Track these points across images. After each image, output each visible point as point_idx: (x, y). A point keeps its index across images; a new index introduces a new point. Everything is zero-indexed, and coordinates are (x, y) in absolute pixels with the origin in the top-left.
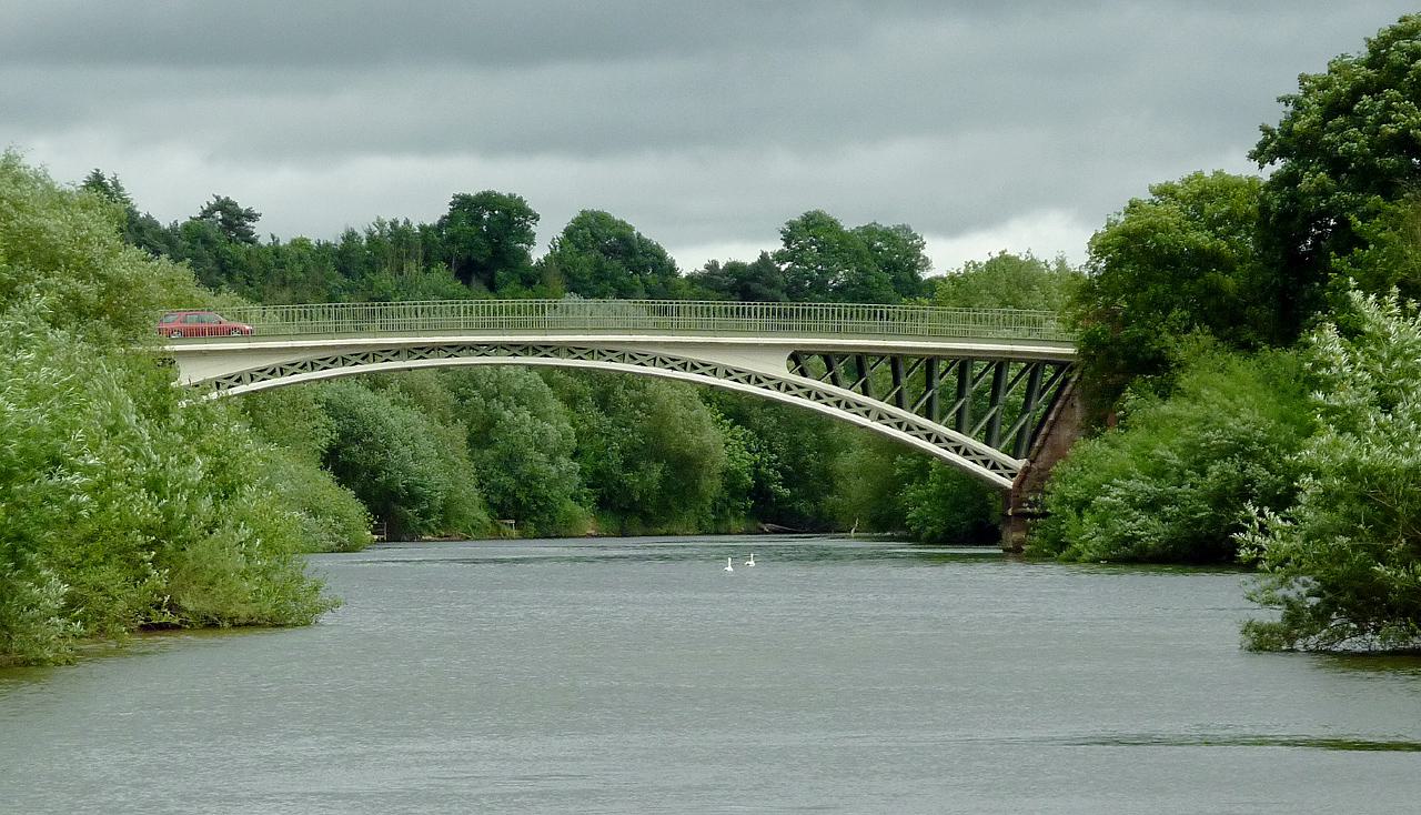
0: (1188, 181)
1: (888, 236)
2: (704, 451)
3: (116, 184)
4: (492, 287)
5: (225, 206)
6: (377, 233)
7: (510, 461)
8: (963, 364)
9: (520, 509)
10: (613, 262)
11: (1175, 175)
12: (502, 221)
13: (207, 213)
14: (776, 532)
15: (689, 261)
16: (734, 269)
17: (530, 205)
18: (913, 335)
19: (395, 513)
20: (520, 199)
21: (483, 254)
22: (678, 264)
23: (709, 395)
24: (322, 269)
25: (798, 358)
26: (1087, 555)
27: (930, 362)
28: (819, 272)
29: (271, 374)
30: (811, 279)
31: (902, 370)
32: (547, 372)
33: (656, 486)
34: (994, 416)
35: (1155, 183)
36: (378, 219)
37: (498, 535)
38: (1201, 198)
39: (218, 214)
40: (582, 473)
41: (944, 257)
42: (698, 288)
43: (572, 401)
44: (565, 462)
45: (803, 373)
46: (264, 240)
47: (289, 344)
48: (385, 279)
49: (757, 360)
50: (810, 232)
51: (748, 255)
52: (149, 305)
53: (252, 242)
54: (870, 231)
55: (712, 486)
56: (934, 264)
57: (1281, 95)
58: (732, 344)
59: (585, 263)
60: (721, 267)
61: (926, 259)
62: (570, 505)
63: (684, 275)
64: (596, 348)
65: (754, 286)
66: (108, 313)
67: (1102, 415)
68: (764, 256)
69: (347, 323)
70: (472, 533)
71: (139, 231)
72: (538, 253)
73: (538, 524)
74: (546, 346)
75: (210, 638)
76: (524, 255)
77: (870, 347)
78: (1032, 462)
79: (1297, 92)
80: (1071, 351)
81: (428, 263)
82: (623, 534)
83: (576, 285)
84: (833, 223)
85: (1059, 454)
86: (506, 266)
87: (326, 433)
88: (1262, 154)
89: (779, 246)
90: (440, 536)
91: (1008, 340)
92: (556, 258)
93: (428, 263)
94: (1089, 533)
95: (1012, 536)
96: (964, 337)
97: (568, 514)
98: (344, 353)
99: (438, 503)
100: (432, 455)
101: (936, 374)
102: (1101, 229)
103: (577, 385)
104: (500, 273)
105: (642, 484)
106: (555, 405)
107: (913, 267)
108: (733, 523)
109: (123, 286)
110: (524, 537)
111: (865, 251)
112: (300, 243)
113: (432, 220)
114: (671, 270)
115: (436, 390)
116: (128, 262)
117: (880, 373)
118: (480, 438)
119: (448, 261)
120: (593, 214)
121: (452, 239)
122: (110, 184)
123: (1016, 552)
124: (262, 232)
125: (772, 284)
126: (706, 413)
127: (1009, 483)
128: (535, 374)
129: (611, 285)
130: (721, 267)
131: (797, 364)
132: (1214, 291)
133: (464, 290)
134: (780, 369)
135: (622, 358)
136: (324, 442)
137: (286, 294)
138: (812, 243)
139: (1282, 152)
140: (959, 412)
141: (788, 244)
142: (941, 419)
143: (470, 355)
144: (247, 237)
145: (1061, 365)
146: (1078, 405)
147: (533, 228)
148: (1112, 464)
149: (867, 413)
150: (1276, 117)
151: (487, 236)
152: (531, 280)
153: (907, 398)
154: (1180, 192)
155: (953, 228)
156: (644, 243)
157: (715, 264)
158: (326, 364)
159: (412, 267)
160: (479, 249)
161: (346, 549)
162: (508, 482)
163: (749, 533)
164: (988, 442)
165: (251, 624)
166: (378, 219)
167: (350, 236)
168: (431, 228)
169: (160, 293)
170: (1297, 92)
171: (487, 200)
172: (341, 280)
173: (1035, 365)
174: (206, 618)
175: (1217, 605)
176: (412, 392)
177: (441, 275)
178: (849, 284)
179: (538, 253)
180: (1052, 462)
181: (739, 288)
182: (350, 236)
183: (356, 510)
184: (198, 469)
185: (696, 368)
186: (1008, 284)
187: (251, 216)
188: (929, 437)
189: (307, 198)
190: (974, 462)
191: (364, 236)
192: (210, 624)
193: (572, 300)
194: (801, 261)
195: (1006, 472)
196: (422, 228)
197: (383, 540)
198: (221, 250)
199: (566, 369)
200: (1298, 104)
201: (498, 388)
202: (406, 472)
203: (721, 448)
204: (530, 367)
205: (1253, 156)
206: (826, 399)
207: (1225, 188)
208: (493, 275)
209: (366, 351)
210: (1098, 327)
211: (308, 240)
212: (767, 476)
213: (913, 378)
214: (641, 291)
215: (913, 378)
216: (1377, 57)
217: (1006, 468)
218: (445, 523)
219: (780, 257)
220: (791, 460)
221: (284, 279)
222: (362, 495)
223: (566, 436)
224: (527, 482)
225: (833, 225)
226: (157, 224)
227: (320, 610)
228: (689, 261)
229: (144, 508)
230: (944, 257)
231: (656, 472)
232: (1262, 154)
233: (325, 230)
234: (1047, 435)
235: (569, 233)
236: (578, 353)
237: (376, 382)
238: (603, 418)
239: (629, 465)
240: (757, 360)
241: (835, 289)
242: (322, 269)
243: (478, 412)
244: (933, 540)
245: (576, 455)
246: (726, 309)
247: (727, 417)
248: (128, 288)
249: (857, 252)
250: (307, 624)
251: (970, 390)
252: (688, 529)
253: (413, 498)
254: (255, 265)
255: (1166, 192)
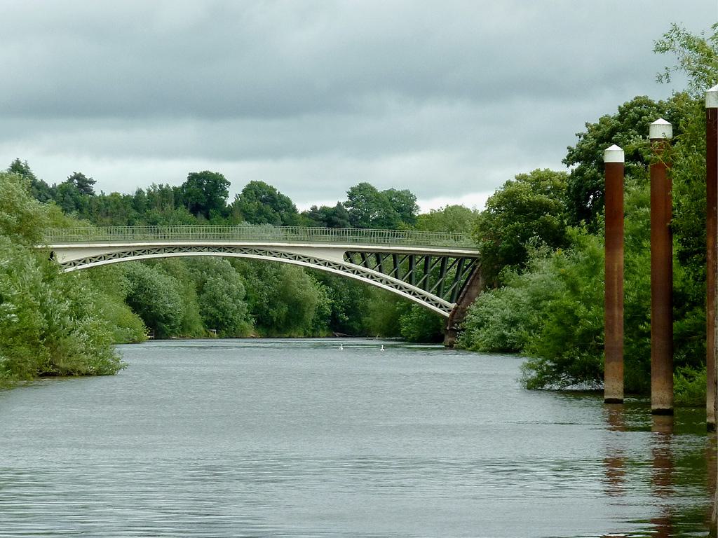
0: (533, 174)
1: (399, 195)
2: (307, 299)
3: (27, 167)
4: (208, 217)
5: (79, 177)
6: (152, 191)
7: (213, 300)
8: (427, 257)
9: (219, 325)
10: (266, 205)
11: (527, 171)
12: (213, 185)
13: (71, 180)
14: (340, 336)
15: (303, 207)
16: (324, 210)
17: (226, 177)
18: (407, 245)
19: (158, 325)
20: (221, 175)
21: (203, 201)
22: (297, 207)
23: (309, 271)
24: (125, 207)
25: (349, 255)
26: (482, 348)
27: (411, 257)
28: (366, 212)
29: (99, 259)
30: (361, 215)
31: (398, 261)
32: (232, 260)
33: (283, 317)
34: (441, 282)
35: (517, 174)
36: (153, 184)
37: (208, 337)
38: (538, 181)
39: (76, 181)
40: (248, 308)
41: (424, 207)
42: (307, 219)
43: (244, 273)
44: (241, 303)
45: (351, 262)
46: (98, 194)
47: (88, 246)
48: (156, 213)
49: (329, 255)
50: (362, 193)
51: (332, 204)
52: (41, 225)
53: (93, 194)
54: (391, 192)
55: (311, 316)
56: (421, 209)
57: (577, 133)
58: (334, 248)
59: (253, 206)
60: (318, 209)
61: (417, 206)
62: (243, 323)
63: (300, 213)
64: (254, 248)
65: (334, 218)
66: (25, 230)
67: (494, 283)
68: (339, 204)
69: (138, 235)
70: (196, 336)
71: (39, 190)
72: (230, 201)
73: (227, 332)
74: (230, 247)
75: (71, 379)
76: (223, 202)
77: (399, 250)
78: (458, 305)
79: (585, 131)
80: (478, 252)
81: (177, 204)
82: (268, 337)
83: (248, 217)
84: (372, 188)
85: (472, 300)
86: (214, 207)
87: (128, 286)
88: (569, 161)
89: (347, 199)
90: (180, 337)
91: (446, 247)
92: (238, 204)
93: (177, 204)
94: (480, 336)
95: (448, 339)
96: (428, 245)
97: (242, 327)
98: (133, 249)
99: (179, 322)
100: (174, 296)
101: (414, 262)
102: (492, 194)
103: (247, 265)
104: (211, 211)
105: (277, 314)
106: (236, 275)
107: (411, 210)
108: (321, 332)
109: (30, 217)
110: (221, 337)
111: (387, 200)
112: (115, 195)
113: (179, 185)
114: (294, 210)
115: (181, 266)
116: (32, 205)
117: (372, 260)
118: (200, 290)
119: (186, 204)
120: (257, 183)
121: (189, 194)
122: (24, 166)
123: (451, 346)
124: (97, 190)
125: (342, 217)
126: (308, 278)
127: (448, 315)
128: (226, 261)
129: (265, 217)
130: (318, 209)
131: (348, 257)
132: (546, 225)
133: (194, 219)
134: (339, 259)
135: (266, 253)
136: (125, 293)
137: (108, 220)
138: (362, 198)
139: (578, 159)
140: (425, 281)
141: (351, 198)
142: (416, 284)
143: (194, 251)
144: (89, 192)
145: (473, 258)
146: (481, 278)
147: (228, 189)
148: (493, 305)
149: (381, 281)
150: (574, 143)
151: (205, 193)
152: (227, 214)
153: (401, 273)
154: (529, 179)
155: (431, 194)
156: (281, 196)
157: (316, 208)
158: (126, 254)
159: (169, 207)
160: (201, 198)
161: (134, 342)
162: (213, 311)
163: (328, 337)
164: (438, 295)
165: (88, 374)
166: (153, 184)
167: (139, 192)
168: (179, 188)
169: (47, 220)
170: (585, 131)
171: (206, 175)
172: (134, 213)
173: (461, 259)
174: (68, 371)
175: (512, 368)
176: (167, 268)
177: (182, 211)
178: (380, 218)
179: (230, 201)
180: (468, 304)
181: (328, 220)
182: (139, 192)
183: (140, 324)
184: (65, 307)
185: (316, 262)
186: (452, 220)
187: (92, 182)
188: (410, 292)
189: (121, 173)
190: (431, 304)
191: (146, 192)
192: (69, 374)
193: (246, 225)
194: (357, 207)
195: (446, 309)
196: (174, 188)
197: (153, 339)
198: (76, 197)
199: (241, 258)
200: (585, 137)
201: (206, 266)
202: (165, 308)
203: (315, 295)
204: (224, 258)
205: (564, 162)
206: (362, 274)
207: (550, 175)
208: (208, 212)
209: (144, 249)
210: (488, 242)
211: (119, 194)
212: (337, 310)
213: (405, 265)
214: (279, 221)
215: (405, 265)
216: (623, 112)
217: (95, 257)
218: (185, 331)
219: (347, 204)
220: (349, 303)
221: (107, 213)
222: (143, 317)
223: (240, 289)
224: (223, 311)
225: (372, 189)
226: (47, 185)
227: (118, 369)
228: (303, 207)
229: (39, 321)
230: (424, 207)
231: (285, 310)
232: (569, 161)
233: (127, 188)
234: (466, 292)
235: (245, 191)
236: (245, 251)
237: (149, 263)
238: (260, 282)
239: (271, 304)
240: (329, 255)
241: (373, 220)
242: (125, 207)
243: (200, 276)
244: (413, 341)
245: (246, 299)
246: (343, 231)
247: (319, 281)
248: (32, 218)
249: (384, 202)
250: (113, 374)
251: (430, 271)
252: (299, 334)
253: (167, 320)
254: (94, 206)
255: (522, 178)
